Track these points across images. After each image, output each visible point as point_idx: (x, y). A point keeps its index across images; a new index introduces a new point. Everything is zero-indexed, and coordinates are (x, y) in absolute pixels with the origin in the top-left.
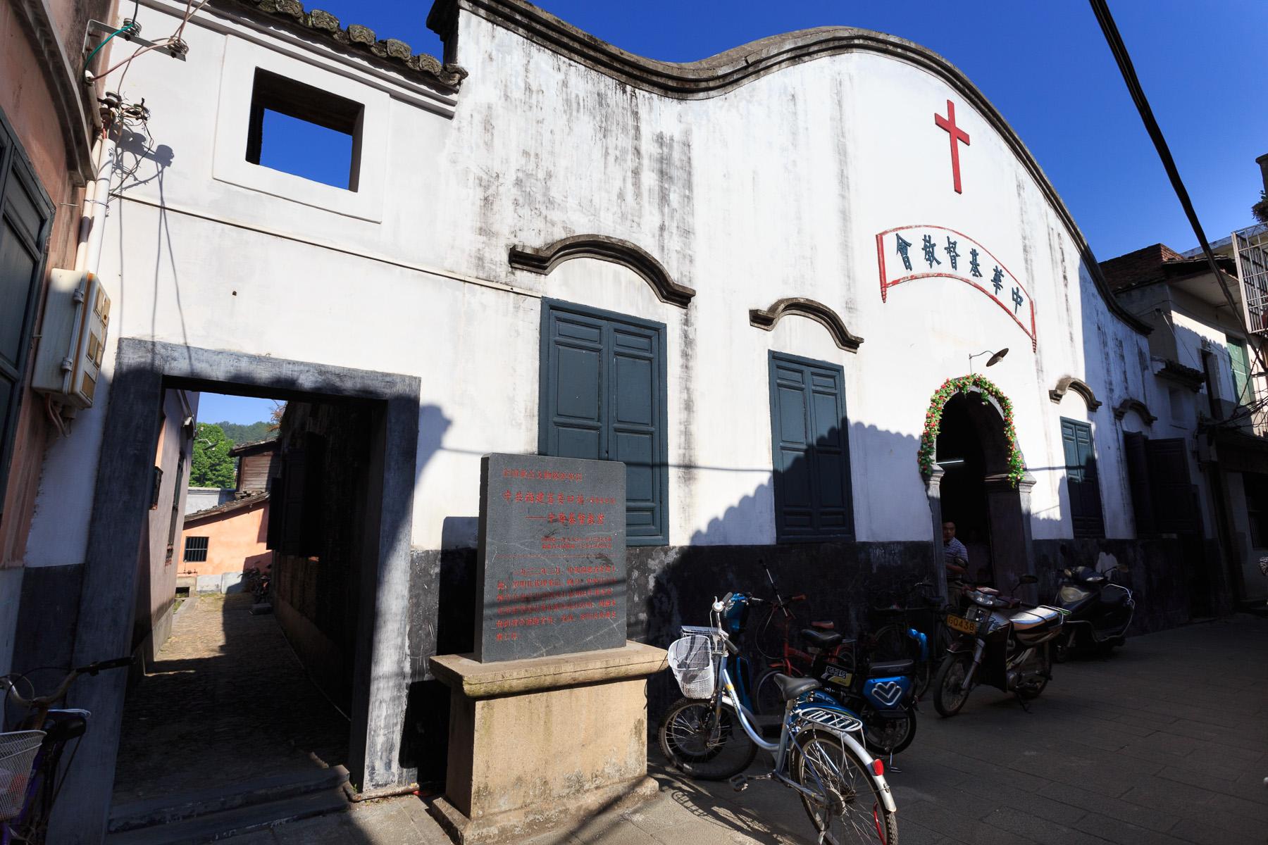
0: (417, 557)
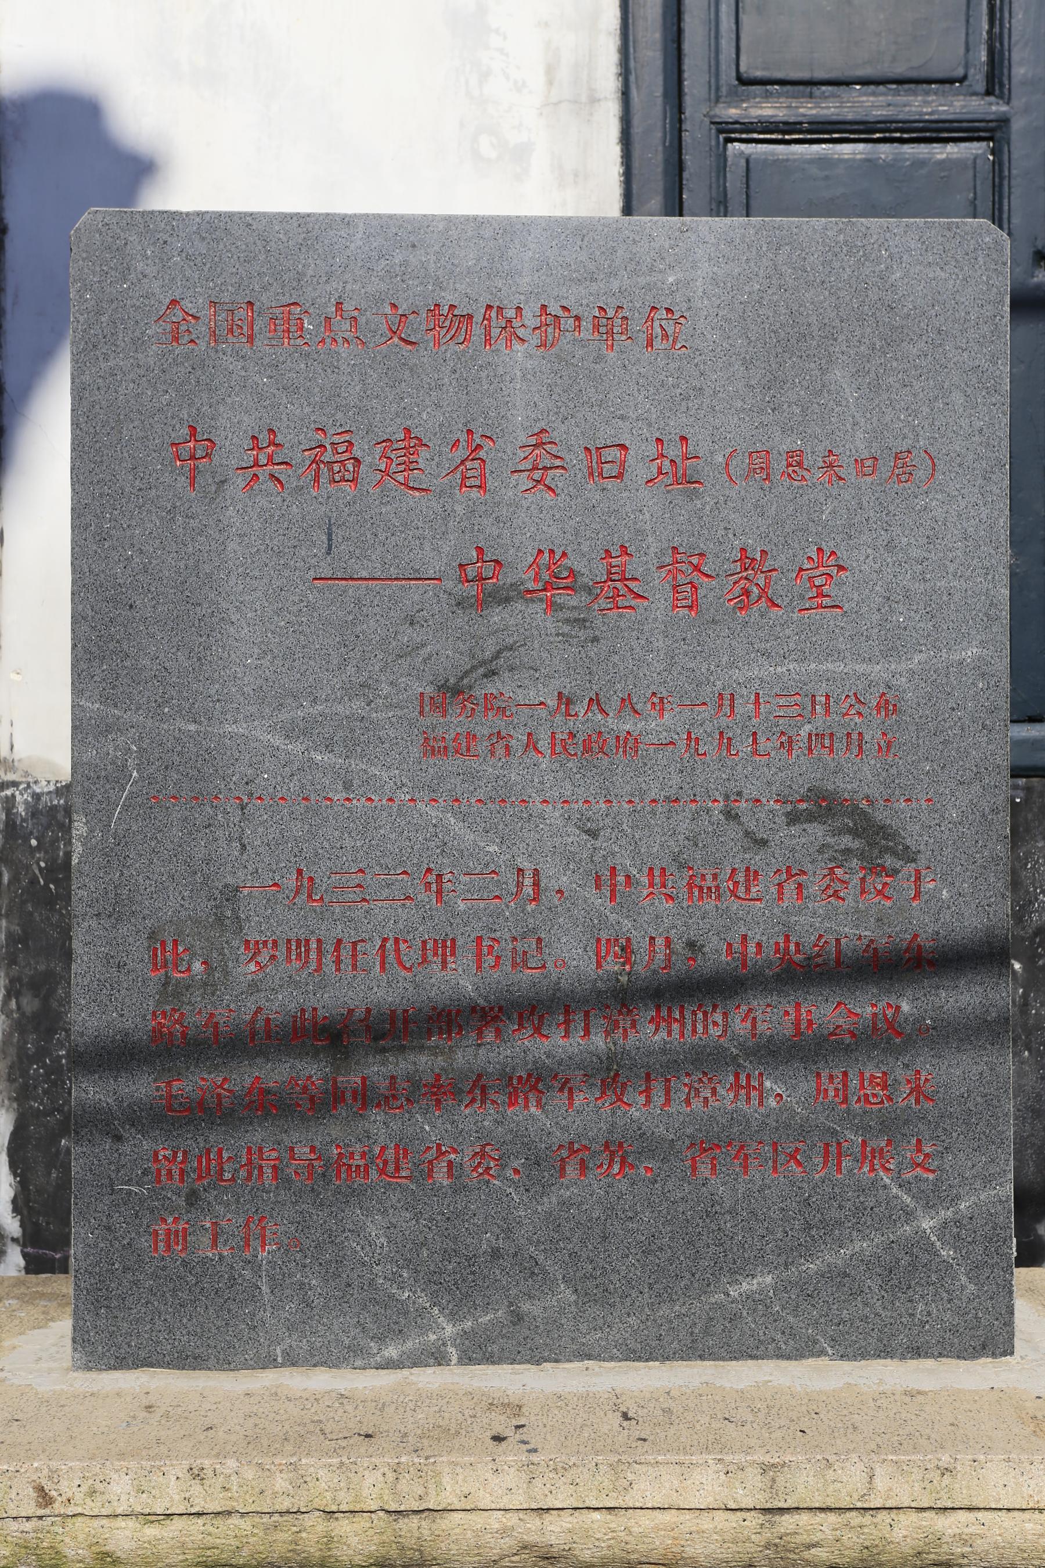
0: (34, 812)
